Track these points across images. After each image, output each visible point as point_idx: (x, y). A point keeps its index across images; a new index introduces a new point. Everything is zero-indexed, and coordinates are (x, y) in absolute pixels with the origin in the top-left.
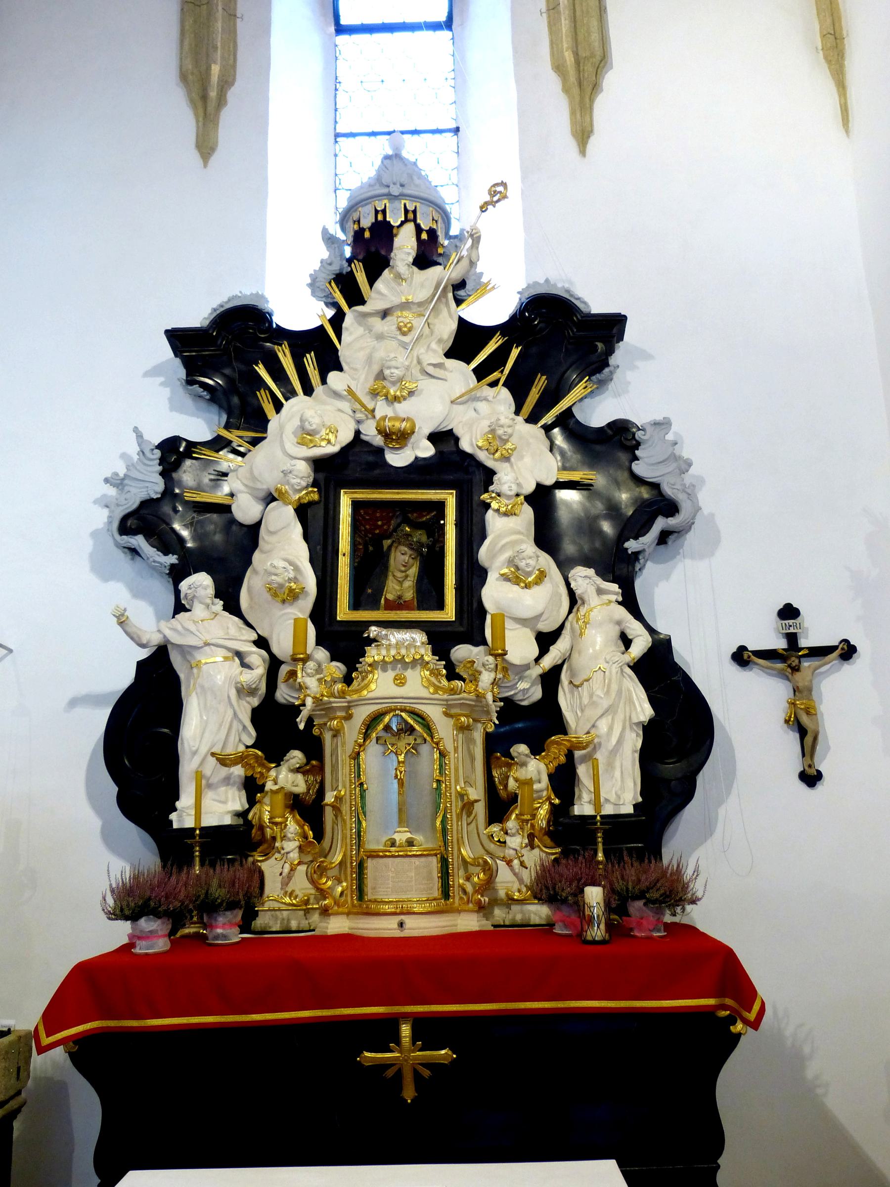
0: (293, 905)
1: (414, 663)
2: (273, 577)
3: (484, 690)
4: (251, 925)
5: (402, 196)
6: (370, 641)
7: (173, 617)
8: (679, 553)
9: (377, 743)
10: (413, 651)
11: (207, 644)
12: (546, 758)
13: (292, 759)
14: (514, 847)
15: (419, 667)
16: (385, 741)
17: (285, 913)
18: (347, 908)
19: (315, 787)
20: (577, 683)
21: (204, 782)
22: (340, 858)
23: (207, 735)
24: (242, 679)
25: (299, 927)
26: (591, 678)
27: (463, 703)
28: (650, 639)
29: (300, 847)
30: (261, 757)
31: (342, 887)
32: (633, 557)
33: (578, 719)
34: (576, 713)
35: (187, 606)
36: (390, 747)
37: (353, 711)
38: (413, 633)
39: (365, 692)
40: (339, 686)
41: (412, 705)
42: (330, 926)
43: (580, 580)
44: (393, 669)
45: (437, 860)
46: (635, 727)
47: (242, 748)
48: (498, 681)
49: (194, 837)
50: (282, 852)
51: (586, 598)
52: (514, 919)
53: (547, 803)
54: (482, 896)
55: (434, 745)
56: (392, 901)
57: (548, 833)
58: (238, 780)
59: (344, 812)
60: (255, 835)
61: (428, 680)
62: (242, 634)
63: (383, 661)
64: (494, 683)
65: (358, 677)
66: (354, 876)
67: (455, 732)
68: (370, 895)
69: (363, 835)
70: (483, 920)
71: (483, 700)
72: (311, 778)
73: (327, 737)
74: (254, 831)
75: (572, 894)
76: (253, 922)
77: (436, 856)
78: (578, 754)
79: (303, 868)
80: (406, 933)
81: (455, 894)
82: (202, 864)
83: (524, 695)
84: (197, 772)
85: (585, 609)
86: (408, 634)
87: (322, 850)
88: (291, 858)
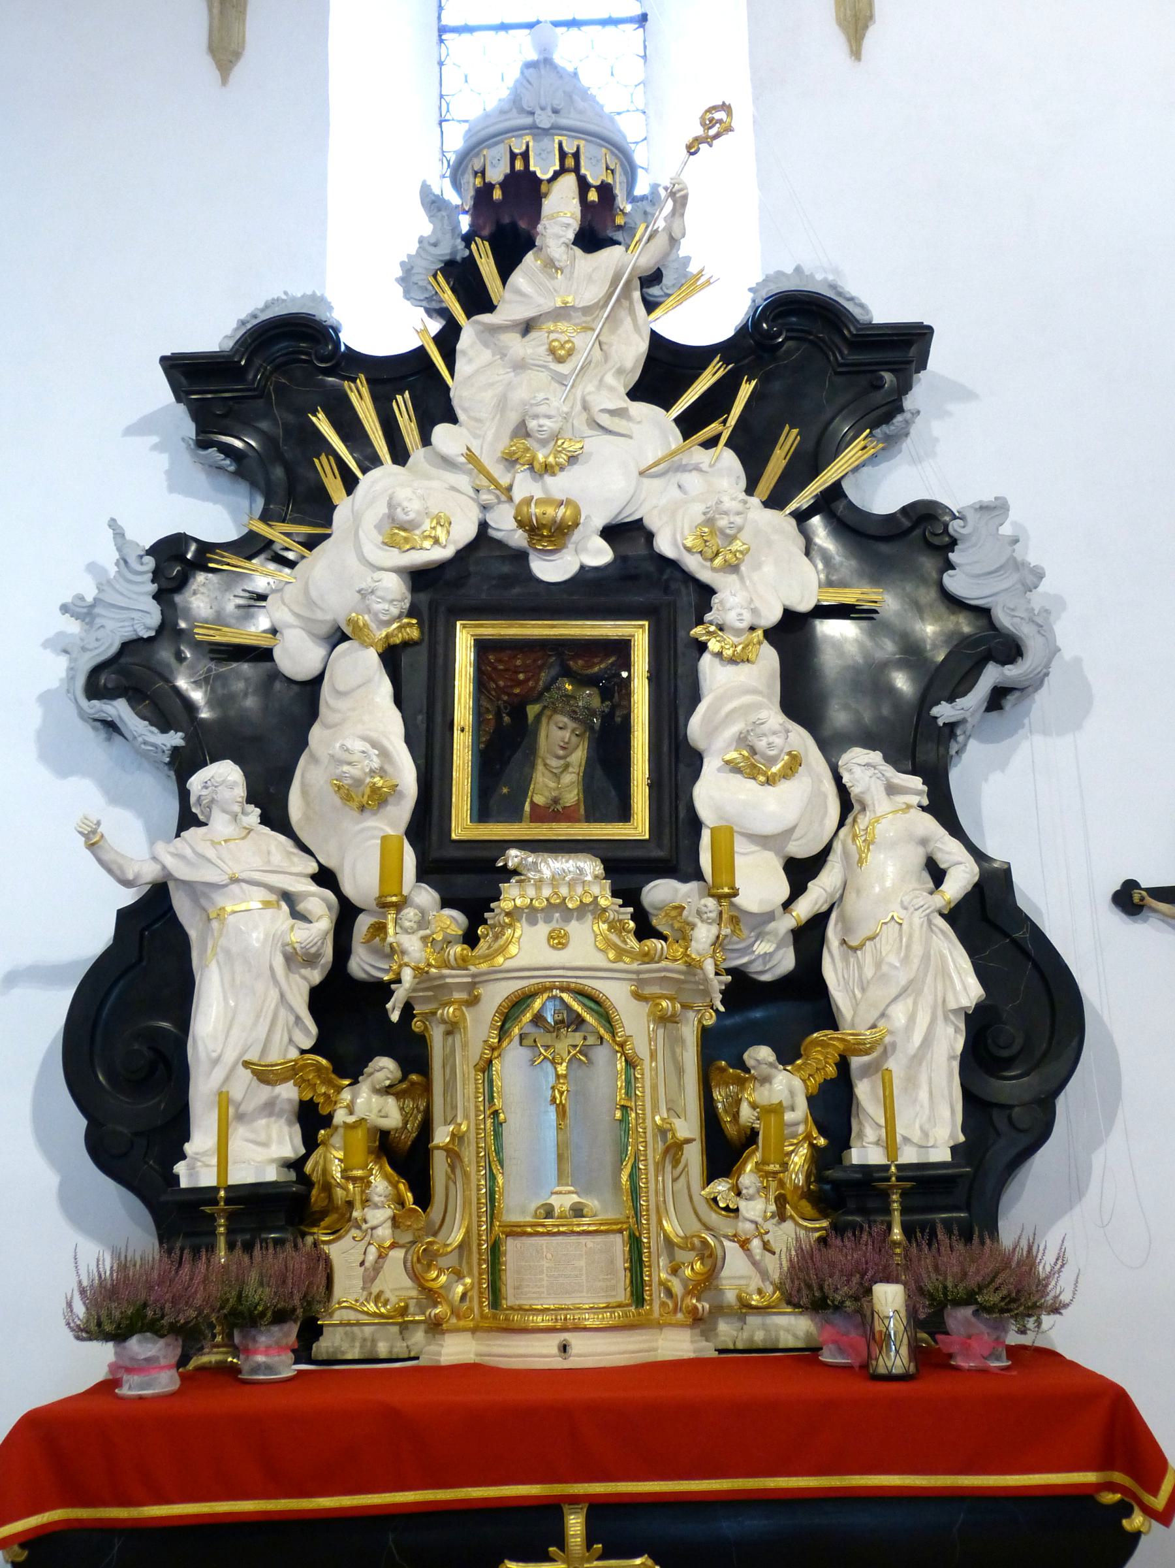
0: (382, 1316)
1: (582, 910)
2: (346, 768)
3: (699, 955)
5: (556, 129)
6: (508, 874)
7: (178, 835)
8: (1023, 726)
9: (521, 1044)
10: (580, 890)
11: (235, 880)
12: (803, 1069)
13: (378, 1071)
14: (753, 1218)
15: (590, 917)
16: (535, 1041)
19: (416, 1118)
20: (854, 943)
21: (231, 1110)
22: (460, 1237)
23: (235, 1032)
25: (391, 1352)
26: (878, 934)
28: (976, 869)
30: (327, 1068)
31: (464, 1285)
32: (947, 731)
33: (856, 1005)
35: (201, 817)
36: (543, 1051)
39: (500, 959)
40: (458, 949)
41: (579, 981)
42: (444, 1351)
43: (858, 770)
44: (548, 920)
45: (623, 1240)
46: (952, 1017)
47: (293, 1054)
49: (216, 1203)
50: (364, 1226)
51: (868, 800)
52: (751, 1340)
53: (806, 1145)
54: (698, 1300)
55: (617, 1048)
56: (548, 1309)
57: (808, 1195)
58: (287, 1107)
63: (531, 907)
65: (487, 935)
66: (484, 1266)
67: (652, 1026)
68: (510, 1298)
71: (699, 971)
73: (436, 1036)
74: (314, 1192)
75: (851, 1297)
76: (314, 1345)
77: (622, 1233)
78: (856, 1062)
79: (398, 1254)
80: (573, 1362)
82: (231, 1247)
83: (765, 964)
84: (220, 1094)
85: (867, 819)
86: (571, 861)
87: (429, 1223)
88: (378, 1236)
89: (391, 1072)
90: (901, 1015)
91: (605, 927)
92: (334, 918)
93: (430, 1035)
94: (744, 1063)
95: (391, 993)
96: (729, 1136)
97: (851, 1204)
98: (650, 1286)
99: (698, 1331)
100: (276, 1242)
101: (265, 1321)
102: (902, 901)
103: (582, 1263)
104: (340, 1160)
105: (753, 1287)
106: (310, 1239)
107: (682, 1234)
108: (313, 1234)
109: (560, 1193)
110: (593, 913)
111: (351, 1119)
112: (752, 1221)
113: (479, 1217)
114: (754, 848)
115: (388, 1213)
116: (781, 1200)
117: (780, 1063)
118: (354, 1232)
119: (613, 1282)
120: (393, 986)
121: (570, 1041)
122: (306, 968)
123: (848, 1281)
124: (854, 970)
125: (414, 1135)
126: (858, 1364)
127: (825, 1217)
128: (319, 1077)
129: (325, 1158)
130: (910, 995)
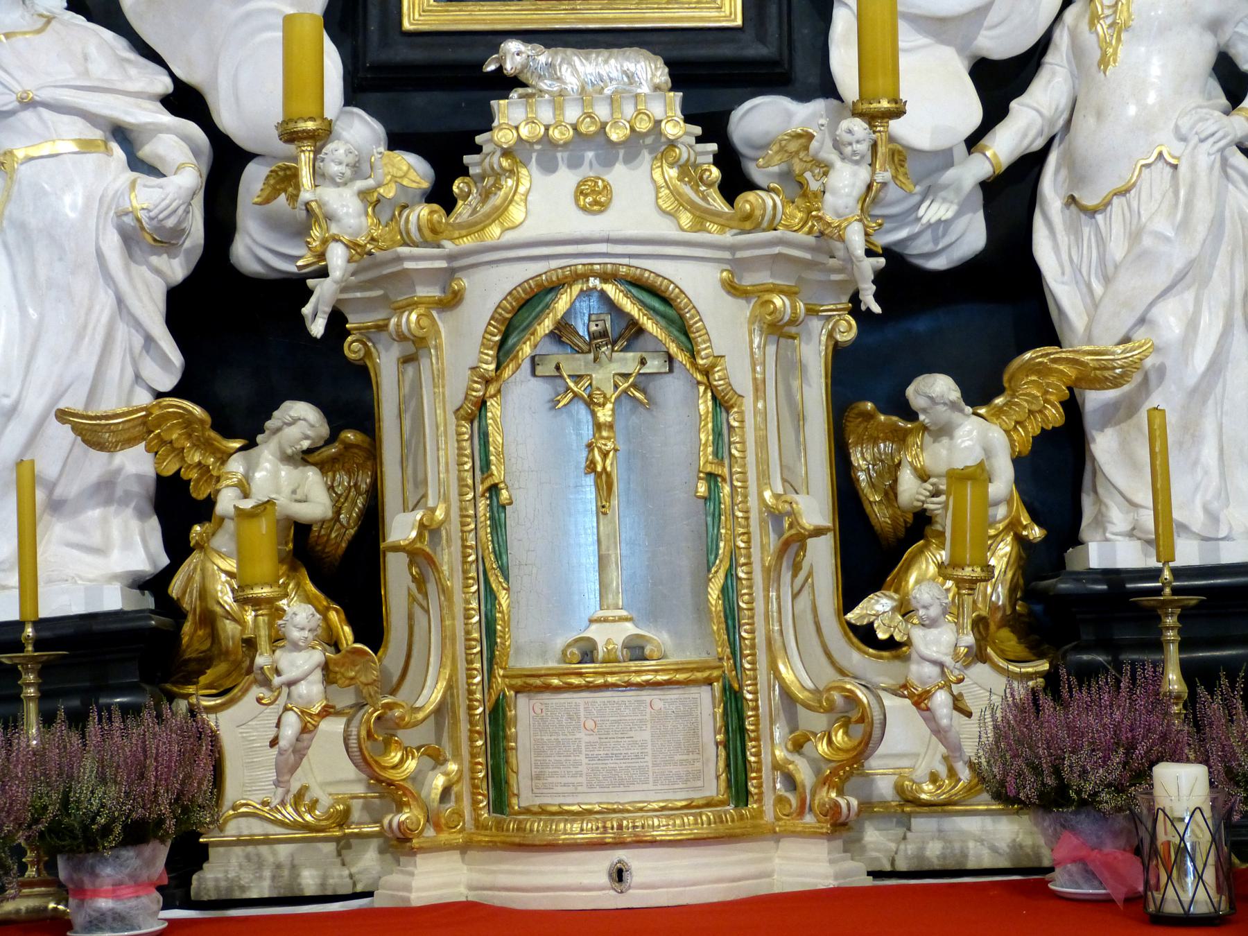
0: (306, 827)
1: (634, 145)
3: (839, 216)
4: (190, 884)
6: (506, 83)
9: (534, 374)
10: (629, 110)
11: (28, 103)
13: (290, 424)
14: (935, 656)
15: (646, 156)
16: (558, 368)
17: (284, 851)
18: (460, 831)
19: (354, 503)
20: (1089, 201)
21: (40, 495)
22: (437, 696)
23: (41, 362)
24: (135, 203)
25: (323, 885)
26: (1134, 185)
27: (779, 255)
29: (326, 667)
30: (202, 422)
31: (446, 774)
33: (1094, 305)
34: (1089, 286)
36: (571, 385)
37: (465, 282)
38: (628, 59)
39: (495, 230)
40: (423, 211)
41: (634, 262)
42: (416, 882)
44: (574, 164)
45: (713, 697)
47: (143, 398)
48: (878, 191)
49: (20, 647)
50: (277, 680)
52: (920, 856)
53: (1009, 539)
54: (841, 793)
55: (699, 377)
56: (590, 812)
57: (1013, 622)
58: (135, 488)
59: (445, 568)
60: (191, 638)
61: (676, 194)
62: (130, 78)
63: (546, 140)
64: (870, 195)
65: (469, 193)
66: (480, 743)
67: (757, 341)
68: (524, 794)
69: (503, 632)
70: (843, 860)
71: (839, 245)
72: (343, 480)
73: (386, 365)
74: (187, 627)
75: (1109, 785)
76: (195, 877)
77: (711, 684)
78: (1093, 400)
79: (333, 727)
80: (634, 898)
81: (764, 788)
82: (47, 719)
83: (936, 241)
84: (19, 463)
86: (612, 61)
87: (384, 672)
88: (300, 696)
89: (312, 426)
90: (1172, 320)
91: (673, 173)
92: (205, 172)
93: (375, 364)
94: (906, 403)
95: (306, 294)
96: (877, 528)
97: (1087, 635)
98: (759, 770)
99: (839, 843)
100: (125, 709)
101: (112, 840)
102: (1177, 128)
103: (646, 735)
104: (230, 574)
105: (922, 771)
106: (182, 705)
107: (809, 684)
108: (186, 696)
109: (606, 620)
110: (652, 150)
111: (247, 504)
112: (934, 662)
113: (470, 662)
114: (923, 40)
115: (317, 656)
116: (980, 624)
117: (967, 404)
118: (256, 691)
119: (698, 765)
120: (310, 282)
121: (616, 368)
122: (159, 255)
123: (1106, 759)
124: (1090, 247)
125: (352, 532)
126: (1122, 897)
127: (1040, 656)
128: (189, 436)
129: (203, 570)
130: (1189, 287)
